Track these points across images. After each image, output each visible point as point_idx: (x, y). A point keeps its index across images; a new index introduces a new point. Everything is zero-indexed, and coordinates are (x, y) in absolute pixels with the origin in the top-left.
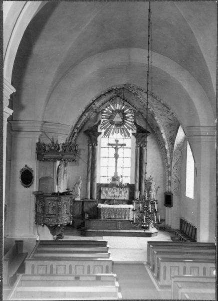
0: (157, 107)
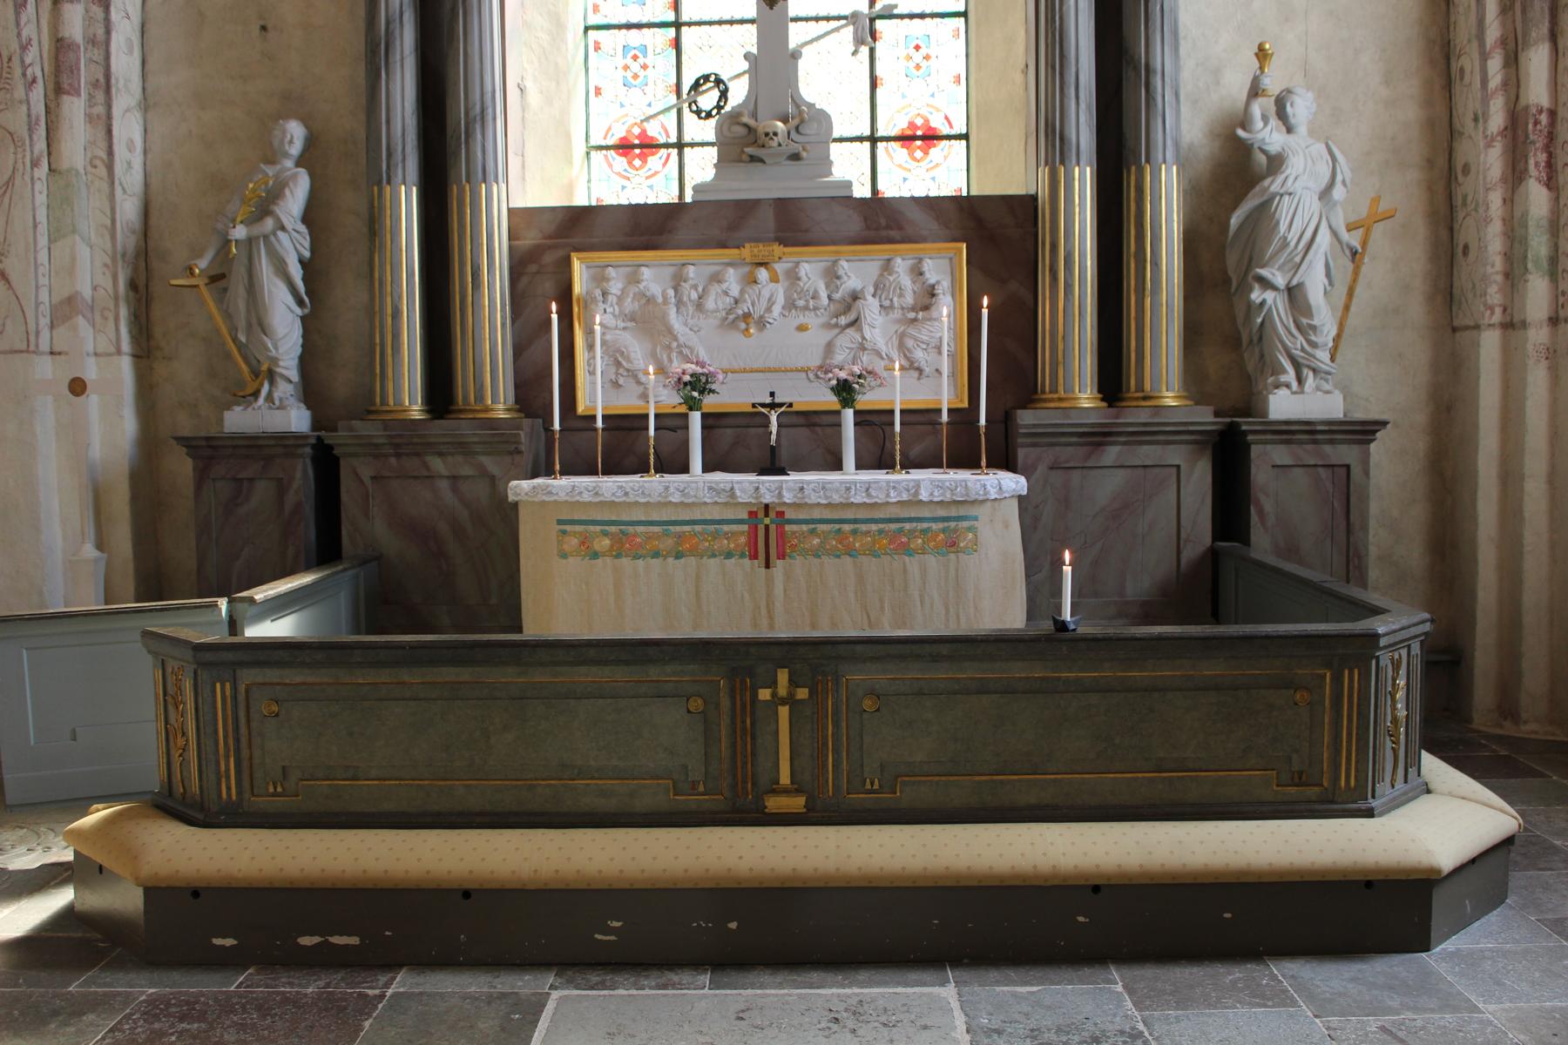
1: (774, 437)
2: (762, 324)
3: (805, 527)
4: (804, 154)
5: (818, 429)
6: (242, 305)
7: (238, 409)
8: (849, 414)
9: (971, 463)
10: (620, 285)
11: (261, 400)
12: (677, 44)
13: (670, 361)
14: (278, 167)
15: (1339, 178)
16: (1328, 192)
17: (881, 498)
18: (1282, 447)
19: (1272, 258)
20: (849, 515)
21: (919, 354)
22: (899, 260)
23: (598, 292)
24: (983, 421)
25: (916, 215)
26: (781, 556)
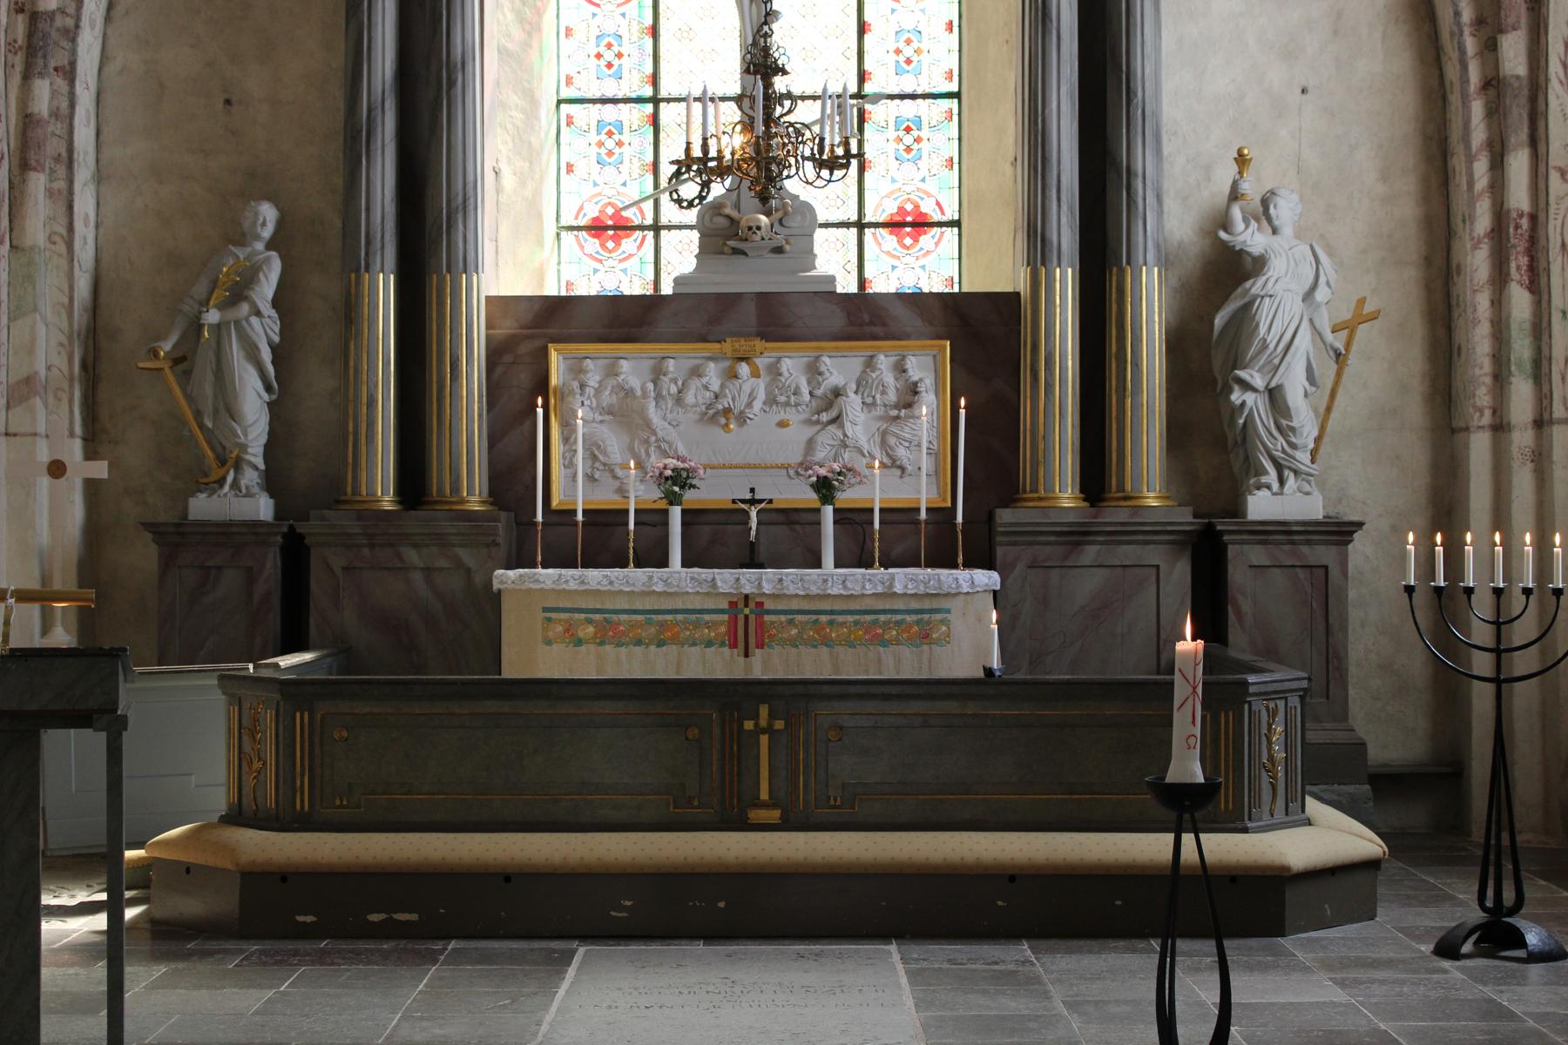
1: (753, 533)
2: (742, 419)
3: (783, 618)
4: (787, 248)
5: (798, 527)
6: (209, 390)
7: (202, 496)
8: (828, 512)
10: (598, 378)
11: (227, 488)
12: (655, 121)
13: (648, 455)
14: (249, 250)
15: (1322, 279)
16: (1322, 294)
17: (857, 590)
18: (1259, 547)
19: (1252, 358)
20: (825, 606)
21: (901, 452)
22: (882, 357)
23: (576, 384)
24: (960, 518)
25: (899, 311)
26: (760, 645)
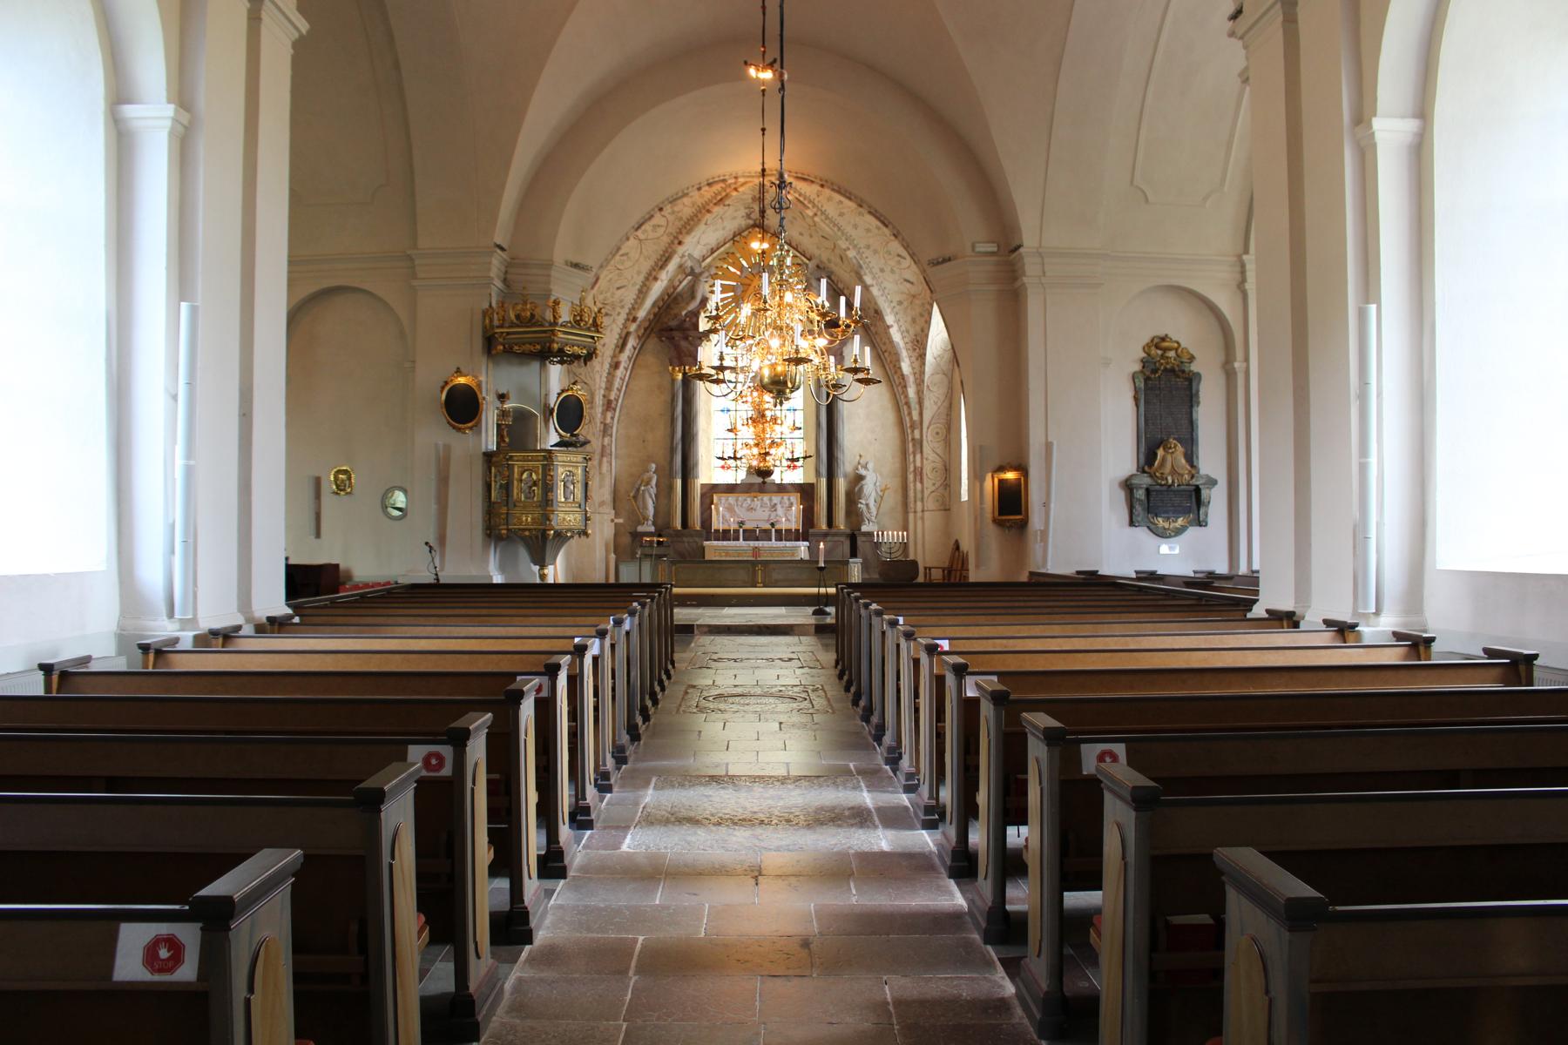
0: (868, 247)
9: (797, 540)
